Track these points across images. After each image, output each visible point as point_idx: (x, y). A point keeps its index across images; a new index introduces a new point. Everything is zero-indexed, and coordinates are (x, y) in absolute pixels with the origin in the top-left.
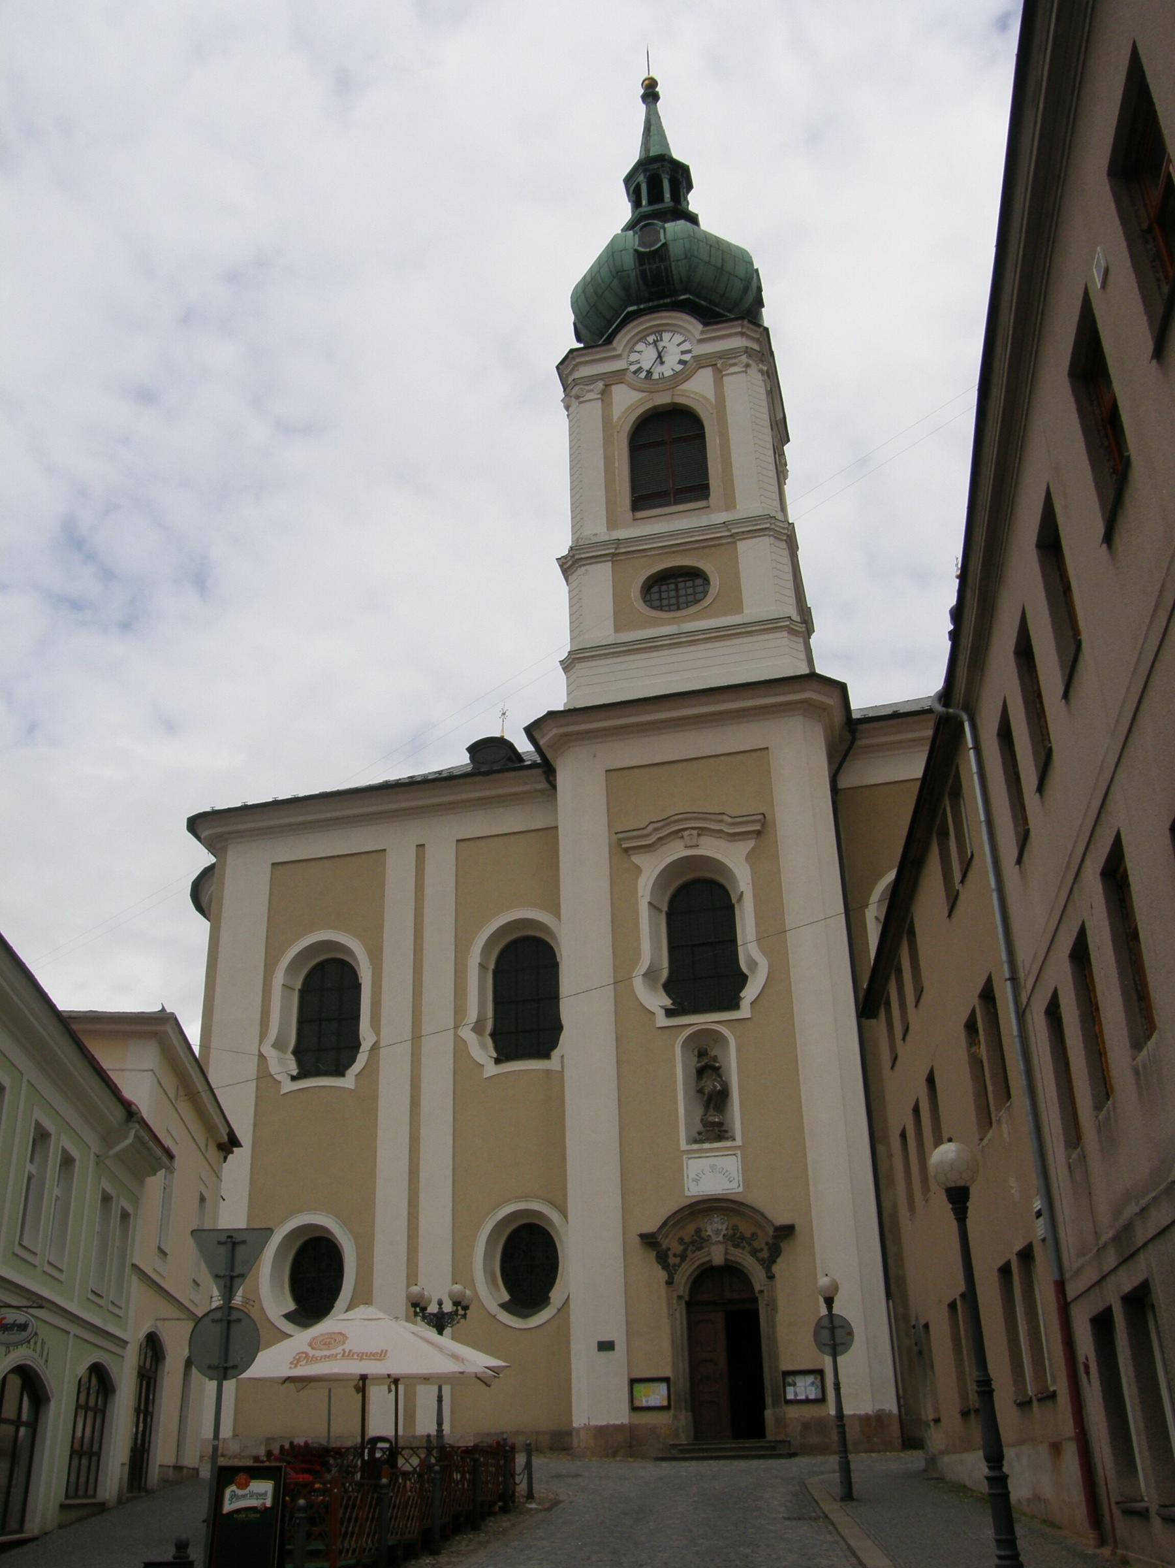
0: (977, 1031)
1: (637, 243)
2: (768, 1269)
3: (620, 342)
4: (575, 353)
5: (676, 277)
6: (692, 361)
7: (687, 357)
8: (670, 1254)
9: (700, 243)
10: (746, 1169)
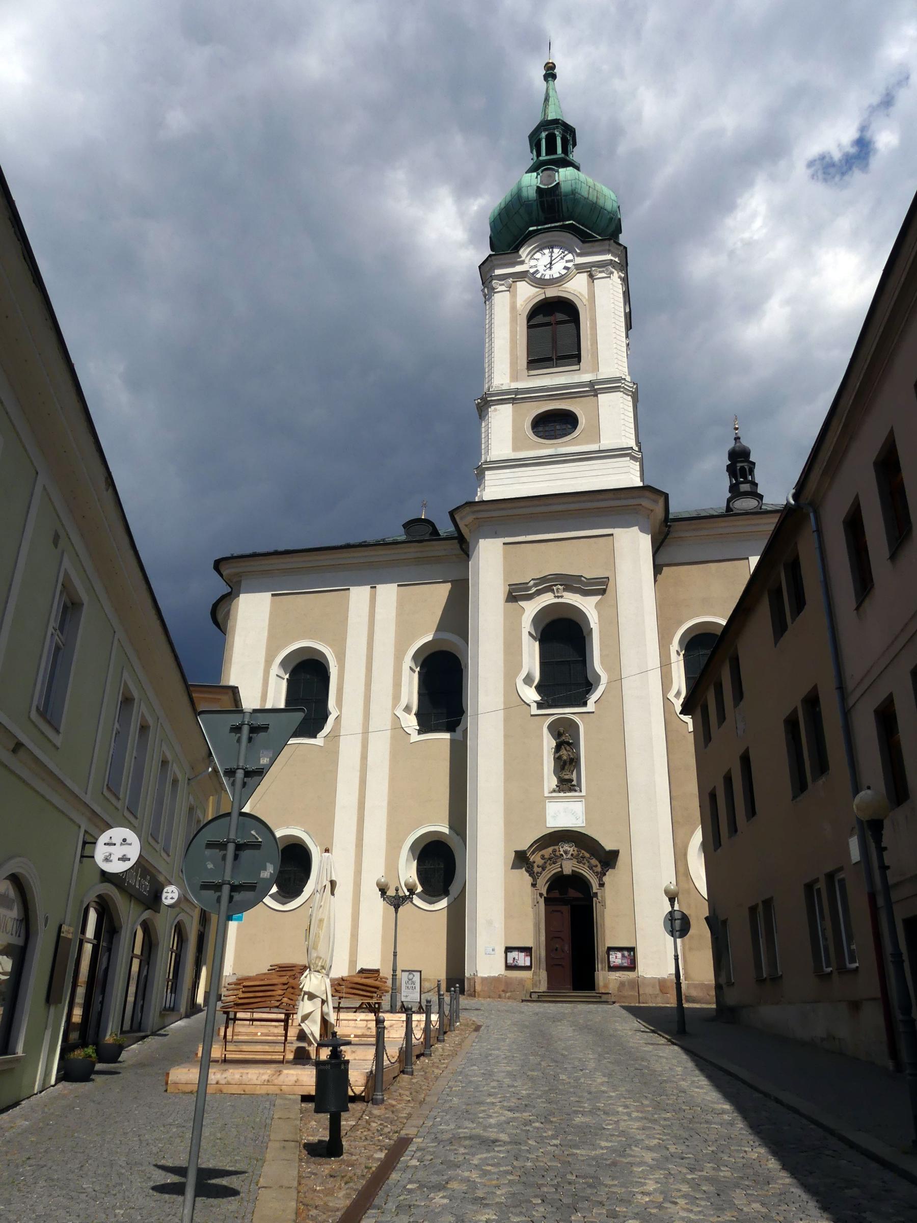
1: (539, 181)
2: (600, 879)
3: (524, 252)
6: (573, 267)
7: (570, 265)
8: (535, 865)
9: (583, 184)
10: (588, 811)
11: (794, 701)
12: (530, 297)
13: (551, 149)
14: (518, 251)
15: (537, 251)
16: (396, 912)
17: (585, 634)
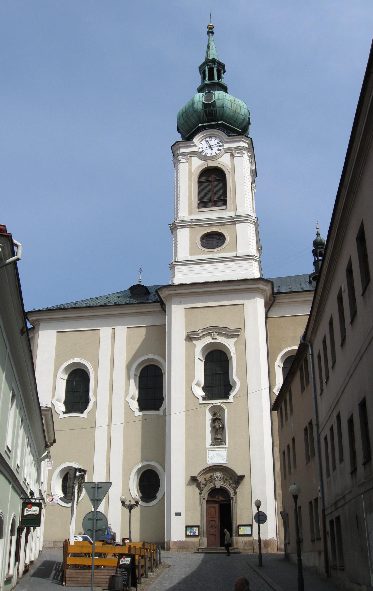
0: (307, 431)
2: (235, 490)
3: (196, 140)
4: (179, 143)
5: (218, 114)
7: (221, 148)
8: (201, 484)
10: (229, 456)
11: (306, 424)
12: (199, 166)
13: (211, 77)
14: (192, 140)
15: (203, 139)
16: (130, 512)
17: (229, 358)
